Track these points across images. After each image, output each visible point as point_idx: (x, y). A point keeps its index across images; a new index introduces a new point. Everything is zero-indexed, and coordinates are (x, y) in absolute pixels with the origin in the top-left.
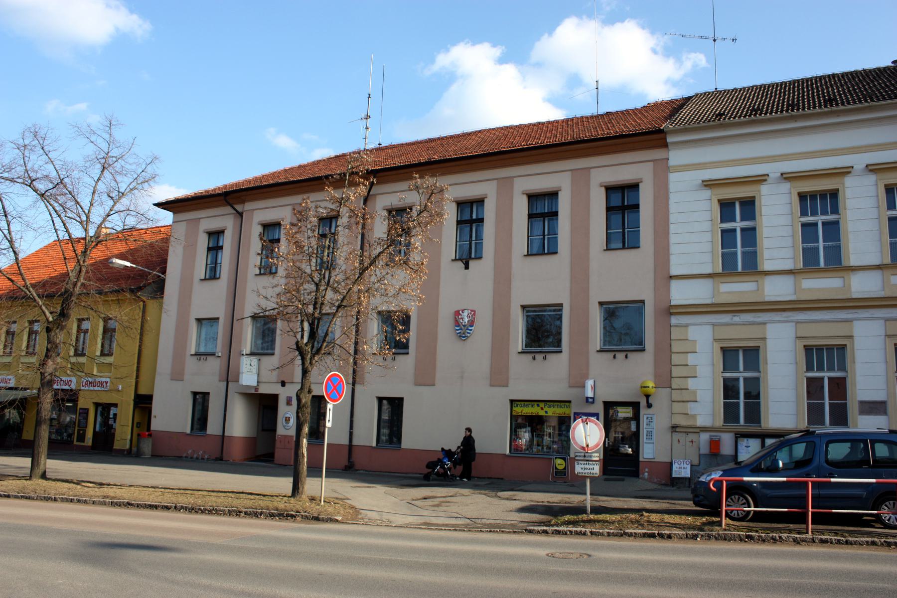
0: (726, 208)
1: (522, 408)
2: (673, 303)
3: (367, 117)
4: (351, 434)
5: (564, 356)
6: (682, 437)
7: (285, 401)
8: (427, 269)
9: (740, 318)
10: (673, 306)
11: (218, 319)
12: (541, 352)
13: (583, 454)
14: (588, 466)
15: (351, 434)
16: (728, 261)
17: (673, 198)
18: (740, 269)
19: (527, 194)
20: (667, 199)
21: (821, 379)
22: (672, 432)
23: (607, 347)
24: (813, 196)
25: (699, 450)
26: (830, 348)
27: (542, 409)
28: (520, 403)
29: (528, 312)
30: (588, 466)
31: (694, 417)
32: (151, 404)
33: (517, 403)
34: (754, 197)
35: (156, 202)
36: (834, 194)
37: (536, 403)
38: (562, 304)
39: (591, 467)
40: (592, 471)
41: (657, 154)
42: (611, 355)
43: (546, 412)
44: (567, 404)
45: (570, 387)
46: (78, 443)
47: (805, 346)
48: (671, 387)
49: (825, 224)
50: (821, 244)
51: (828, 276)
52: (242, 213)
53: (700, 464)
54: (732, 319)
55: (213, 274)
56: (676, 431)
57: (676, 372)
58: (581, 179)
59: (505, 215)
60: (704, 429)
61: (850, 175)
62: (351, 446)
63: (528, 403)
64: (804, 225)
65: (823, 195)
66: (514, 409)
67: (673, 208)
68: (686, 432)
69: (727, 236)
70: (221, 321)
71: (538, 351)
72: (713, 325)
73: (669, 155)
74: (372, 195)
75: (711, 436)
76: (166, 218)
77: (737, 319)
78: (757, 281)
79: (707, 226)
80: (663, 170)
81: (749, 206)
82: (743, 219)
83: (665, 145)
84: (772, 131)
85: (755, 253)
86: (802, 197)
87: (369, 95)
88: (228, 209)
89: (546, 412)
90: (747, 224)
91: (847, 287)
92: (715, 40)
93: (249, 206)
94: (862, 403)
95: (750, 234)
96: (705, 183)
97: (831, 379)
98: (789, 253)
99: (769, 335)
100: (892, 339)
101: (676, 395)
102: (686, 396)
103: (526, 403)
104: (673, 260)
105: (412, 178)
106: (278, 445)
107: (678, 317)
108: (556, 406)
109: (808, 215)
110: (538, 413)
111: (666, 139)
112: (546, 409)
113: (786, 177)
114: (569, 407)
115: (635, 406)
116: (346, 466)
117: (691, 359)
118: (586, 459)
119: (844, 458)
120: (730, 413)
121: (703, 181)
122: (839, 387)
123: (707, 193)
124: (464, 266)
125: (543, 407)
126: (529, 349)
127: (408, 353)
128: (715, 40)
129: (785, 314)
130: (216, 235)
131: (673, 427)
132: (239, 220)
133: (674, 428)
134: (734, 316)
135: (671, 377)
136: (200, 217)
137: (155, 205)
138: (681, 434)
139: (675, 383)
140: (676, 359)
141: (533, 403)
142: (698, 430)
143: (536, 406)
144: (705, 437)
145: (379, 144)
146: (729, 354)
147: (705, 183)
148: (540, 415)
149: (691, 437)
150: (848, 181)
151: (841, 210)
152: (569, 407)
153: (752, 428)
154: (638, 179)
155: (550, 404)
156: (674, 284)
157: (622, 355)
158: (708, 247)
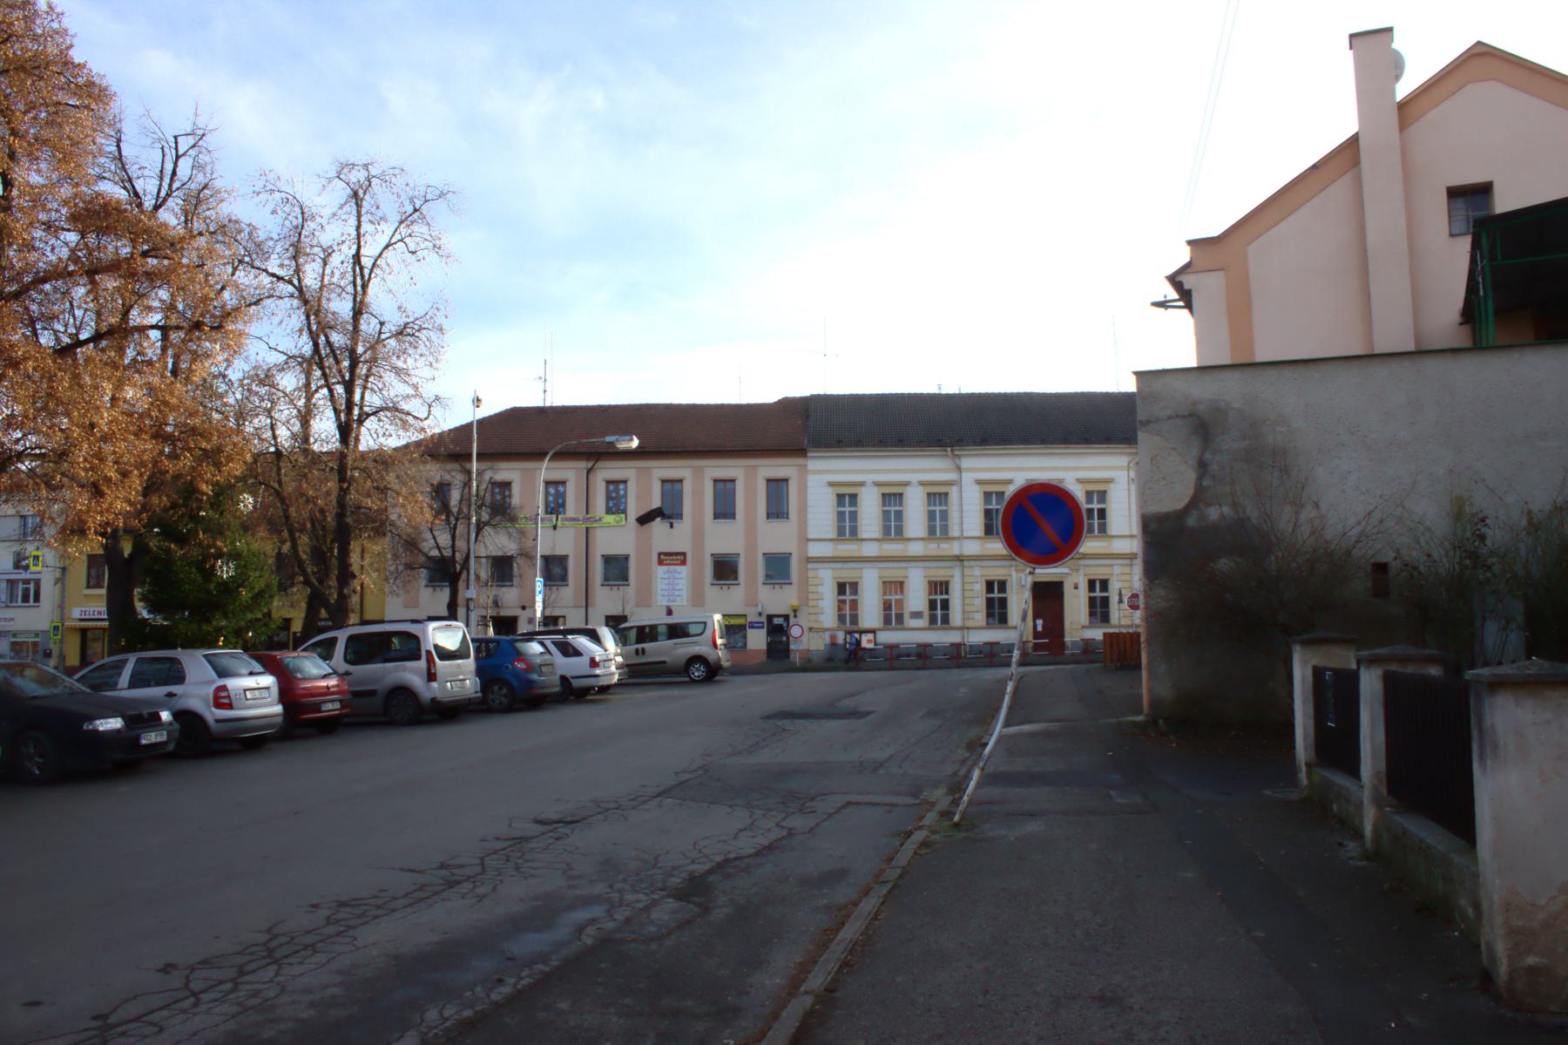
0: (840, 497)
2: (810, 555)
6: (815, 634)
7: (526, 621)
8: (171, 542)
16: (841, 531)
17: (810, 491)
36: (901, 495)
41: (799, 461)
50: (893, 523)
57: (811, 596)
58: (698, 471)
59: (699, 494)
60: (827, 630)
64: (838, 512)
67: (810, 497)
69: (841, 515)
77: (846, 566)
80: (804, 471)
81: (854, 497)
82: (850, 506)
84: (858, 456)
85: (947, 526)
86: (929, 494)
90: (852, 509)
95: (854, 516)
97: (941, 600)
101: (811, 610)
104: (809, 529)
105: (946, 451)
113: (922, 484)
115: (786, 617)
117: (820, 589)
120: (841, 618)
123: (830, 490)
126: (606, 583)
129: (873, 563)
139: (811, 603)
140: (811, 589)
144: (827, 634)
146: (841, 588)
149: (821, 634)
150: (909, 489)
151: (904, 505)
153: (855, 628)
156: (810, 544)
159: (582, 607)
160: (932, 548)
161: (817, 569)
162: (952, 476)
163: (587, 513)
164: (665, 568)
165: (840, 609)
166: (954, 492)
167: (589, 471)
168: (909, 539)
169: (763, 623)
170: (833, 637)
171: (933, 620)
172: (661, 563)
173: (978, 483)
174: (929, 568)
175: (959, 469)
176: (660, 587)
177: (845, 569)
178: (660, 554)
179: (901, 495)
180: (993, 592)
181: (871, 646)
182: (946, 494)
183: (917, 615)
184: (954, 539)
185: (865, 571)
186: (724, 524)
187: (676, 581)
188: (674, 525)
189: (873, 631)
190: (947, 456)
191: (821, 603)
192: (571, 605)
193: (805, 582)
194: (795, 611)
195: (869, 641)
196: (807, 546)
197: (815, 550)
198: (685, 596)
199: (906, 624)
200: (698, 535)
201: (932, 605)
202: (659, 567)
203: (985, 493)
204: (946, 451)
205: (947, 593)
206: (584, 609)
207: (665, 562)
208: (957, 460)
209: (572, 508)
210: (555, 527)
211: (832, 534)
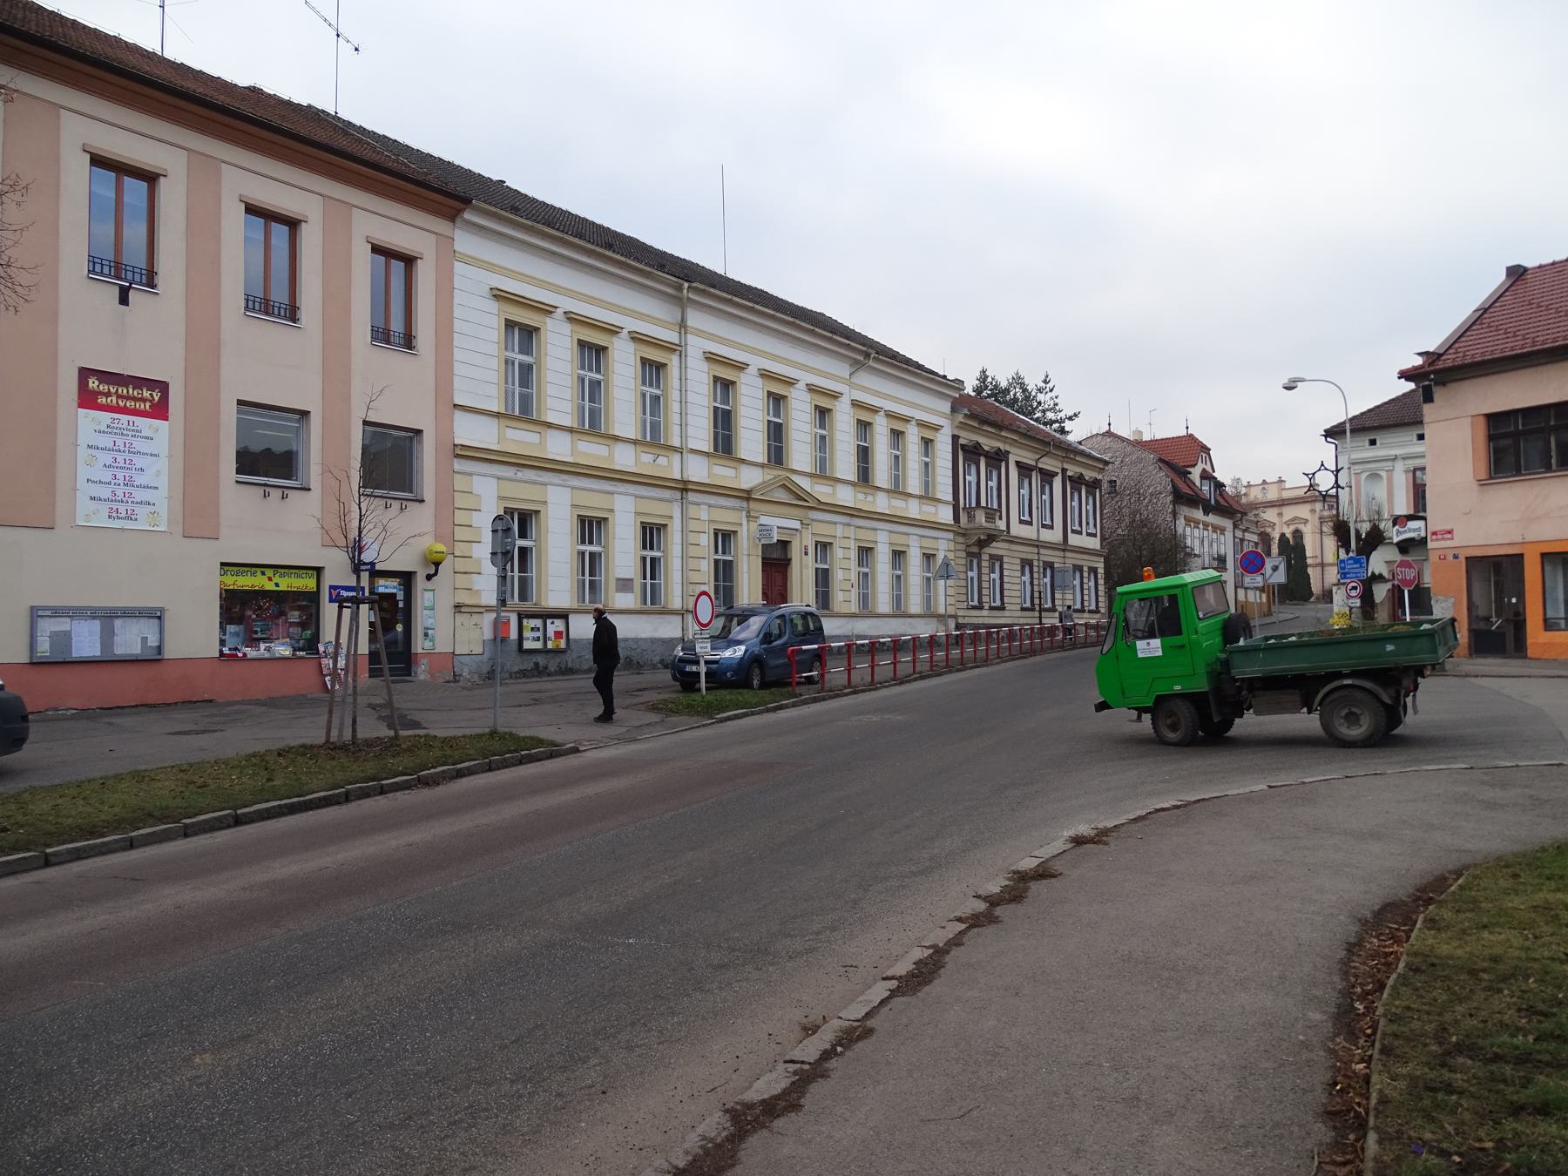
1: (235, 578)
19: (246, 203)
23: (1557, 621)
27: (270, 579)
28: (231, 568)
31: (478, 592)
37: (259, 570)
42: (260, 490)
63: (246, 569)
71: (380, 494)
72: (890, 532)
78: (667, 456)
89: (277, 585)
91: (611, 457)
103: (242, 569)
107: (463, 461)
108: (293, 575)
110: (263, 586)
112: (276, 579)
115: (406, 578)
123: (493, 306)
125: (272, 575)
131: (456, 607)
141: (253, 569)
142: (483, 610)
143: (259, 573)
148: (267, 589)
157: (396, 504)
162: (671, 336)
172: (88, 400)
174: (642, 497)
175: (683, 326)
183: (625, 585)
187: (139, 462)
189: (563, 615)
197: (472, 432)
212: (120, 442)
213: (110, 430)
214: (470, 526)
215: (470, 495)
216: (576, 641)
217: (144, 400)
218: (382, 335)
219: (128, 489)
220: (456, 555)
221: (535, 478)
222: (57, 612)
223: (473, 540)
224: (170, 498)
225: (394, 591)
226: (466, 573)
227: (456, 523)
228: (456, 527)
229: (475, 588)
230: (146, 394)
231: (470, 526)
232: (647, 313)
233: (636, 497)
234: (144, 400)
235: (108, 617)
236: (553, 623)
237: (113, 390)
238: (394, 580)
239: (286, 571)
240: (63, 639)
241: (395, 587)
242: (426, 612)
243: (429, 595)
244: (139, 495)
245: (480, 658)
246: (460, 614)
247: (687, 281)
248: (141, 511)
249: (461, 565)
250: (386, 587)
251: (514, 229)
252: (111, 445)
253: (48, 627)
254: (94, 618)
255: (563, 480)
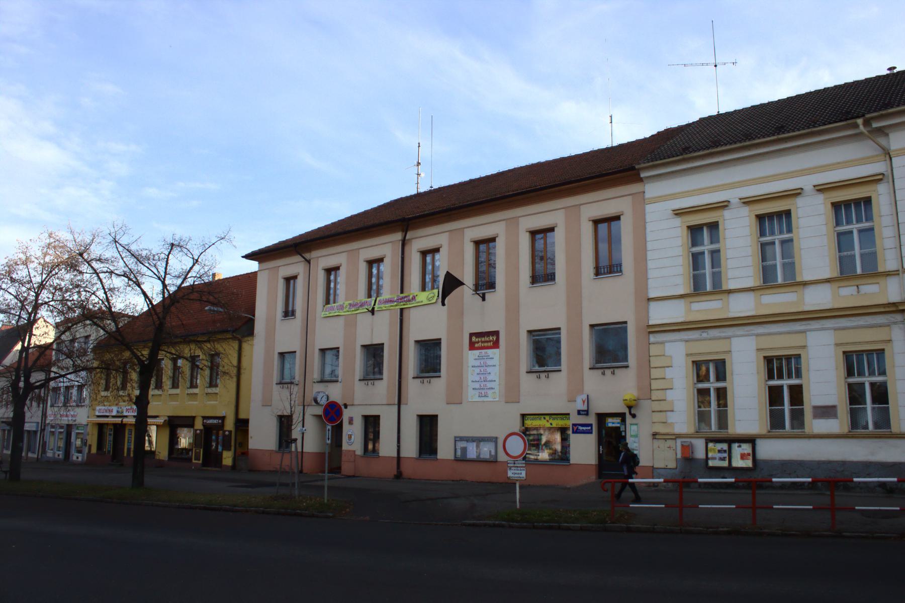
0: (695, 231)
3: (419, 164)
4: (399, 447)
5: (563, 375)
6: (661, 443)
9: (708, 334)
10: (651, 325)
11: (295, 352)
12: (545, 371)
13: (513, 462)
14: (517, 472)
15: (399, 447)
18: (859, 271)
20: (645, 228)
21: (781, 387)
22: (653, 439)
24: (847, 204)
25: (676, 455)
26: (870, 352)
27: (548, 421)
28: (529, 416)
29: (534, 336)
30: (517, 472)
31: (672, 424)
32: (248, 426)
33: (528, 417)
34: (718, 222)
35: (244, 255)
36: (788, 213)
37: (542, 417)
38: (560, 328)
39: (520, 472)
40: (520, 476)
42: (600, 371)
43: (551, 424)
44: (567, 416)
45: (569, 401)
46: (196, 462)
47: (765, 357)
48: (651, 399)
49: (860, 231)
51: (772, 292)
52: (310, 260)
53: (677, 467)
54: (701, 335)
55: (289, 313)
56: (656, 438)
57: (655, 385)
60: (679, 436)
61: (800, 196)
62: (399, 458)
65: (857, 202)
66: (526, 422)
68: (664, 439)
69: (696, 260)
70: (298, 354)
71: (543, 370)
73: (644, 189)
74: (409, 240)
75: (682, 442)
76: (253, 266)
77: (705, 335)
78: (878, 283)
79: (679, 251)
80: (641, 201)
83: (641, 180)
84: (829, 140)
86: (836, 206)
87: (419, 143)
88: (298, 258)
89: (551, 424)
92: (716, 66)
93: (314, 254)
94: (815, 408)
96: (743, 201)
98: (750, 271)
99: (734, 348)
100: (840, 347)
101: (656, 406)
102: (662, 406)
104: (651, 283)
106: (344, 458)
109: (862, 221)
111: (639, 175)
112: (551, 421)
114: (569, 419)
115: (622, 416)
116: (395, 475)
117: (669, 373)
118: (515, 465)
119: (761, 460)
120: (703, 417)
121: (814, 186)
122: (797, 393)
123: (678, 221)
124: (481, 299)
127: (440, 377)
128: (716, 66)
130: (290, 280)
131: (653, 435)
132: (308, 265)
133: (655, 435)
134: (703, 332)
135: (651, 390)
136: (278, 265)
137: (243, 257)
138: (660, 441)
140: (655, 373)
141: (540, 416)
143: (542, 419)
145: (431, 187)
146: (700, 369)
147: (743, 201)
149: (670, 443)
152: (569, 419)
153: (722, 434)
154: (620, 212)
155: (554, 416)
156: (653, 305)
157: (608, 372)
158: (680, 270)
159: (394, 404)
160: (847, 295)
161: (663, 343)
162: (878, 167)
163: (402, 292)
164: (477, 352)
165: (700, 404)
166: (881, 195)
167: (404, 243)
168: (805, 284)
169: (591, 425)
170: (687, 449)
171: (855, 420)
172: (472, 347)
173: (819, 190)
174: (844, 329)
175: (888, 154)
176: (471, 378)
177: (705, 339)
178: (471, 335)
179: (788, 213)
180: (706, 378)
181: (748, 463)
182: (868, 201)
183: (826, 412)
184: (888, 274)
185: (734, 341)
186: (609, 283)
187: (489, 370)
188: (487, 296)
189: (751, 440)
190: (858, 136)
191: (670, 395)
192: (385, 402)
193: (646, 365)
194: (630, 408)
195: (743, 457)
196: (648, 305)
197: (660, 314)
198: (497, 390)
199: (807, 430)
200: (513, 308)
201: (855, 395)
202: (470, 352)
203: (833, 204)
204: (856, 126)
205: (799, 375)
206: (396, 407)
207: (476, 345)
208: (882, 141)
209: (388, 288)
210: (373, 312)
211: (682, 286)
212: (482, 363)
213: (480, 358)
214: (664, 378)
215: (662, 357)
216: (766, 462)
217: (490, 341)
218: (535, 279)
219: (485, 383)
220: (653, 399)
221: (719, 335)
222: (462, 439)
223: (666, 388)
224: (499, 385)
225: (618, 425)
226: (661, 411)
227: (652, 377)
228: (652, 381)
229: (669, 421)
230: (491, 338)
231: (664, 378)
232: (835, 161)
233: (836, 329)
234: (490, 341)
235: (479, 440)
236: (740, 446)
237: (480, 340)
238: (618, 418)
239: (556, 416)
240: (464, 450)
241: (618, 423)
242: (633, 439)
243: (634, 428)
244: (489, 385)
245: (674, 471)
246: (656, 440)
247: (858, 117)
248: (490, 392)
249: (656, 406)
250: (613, 423)
251: (678, 165)
252: (479, 364)
253: (462, 444)
254: (474, 441)
255: (747, 331)
